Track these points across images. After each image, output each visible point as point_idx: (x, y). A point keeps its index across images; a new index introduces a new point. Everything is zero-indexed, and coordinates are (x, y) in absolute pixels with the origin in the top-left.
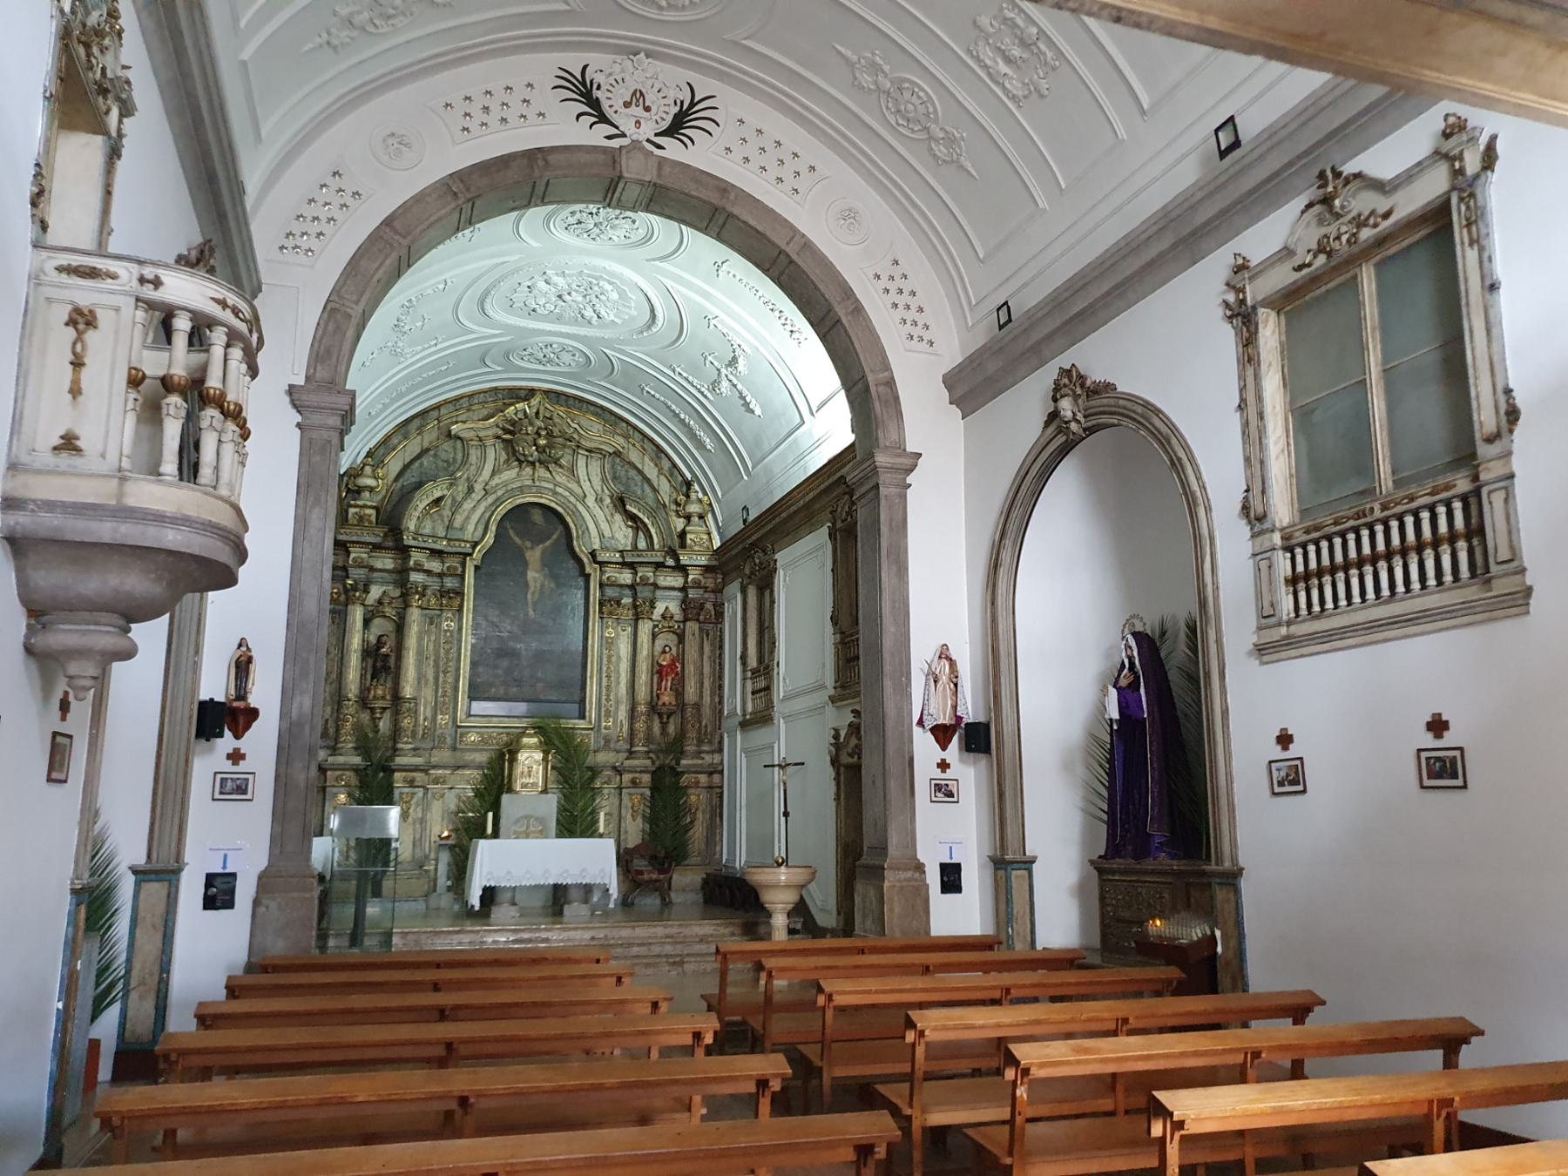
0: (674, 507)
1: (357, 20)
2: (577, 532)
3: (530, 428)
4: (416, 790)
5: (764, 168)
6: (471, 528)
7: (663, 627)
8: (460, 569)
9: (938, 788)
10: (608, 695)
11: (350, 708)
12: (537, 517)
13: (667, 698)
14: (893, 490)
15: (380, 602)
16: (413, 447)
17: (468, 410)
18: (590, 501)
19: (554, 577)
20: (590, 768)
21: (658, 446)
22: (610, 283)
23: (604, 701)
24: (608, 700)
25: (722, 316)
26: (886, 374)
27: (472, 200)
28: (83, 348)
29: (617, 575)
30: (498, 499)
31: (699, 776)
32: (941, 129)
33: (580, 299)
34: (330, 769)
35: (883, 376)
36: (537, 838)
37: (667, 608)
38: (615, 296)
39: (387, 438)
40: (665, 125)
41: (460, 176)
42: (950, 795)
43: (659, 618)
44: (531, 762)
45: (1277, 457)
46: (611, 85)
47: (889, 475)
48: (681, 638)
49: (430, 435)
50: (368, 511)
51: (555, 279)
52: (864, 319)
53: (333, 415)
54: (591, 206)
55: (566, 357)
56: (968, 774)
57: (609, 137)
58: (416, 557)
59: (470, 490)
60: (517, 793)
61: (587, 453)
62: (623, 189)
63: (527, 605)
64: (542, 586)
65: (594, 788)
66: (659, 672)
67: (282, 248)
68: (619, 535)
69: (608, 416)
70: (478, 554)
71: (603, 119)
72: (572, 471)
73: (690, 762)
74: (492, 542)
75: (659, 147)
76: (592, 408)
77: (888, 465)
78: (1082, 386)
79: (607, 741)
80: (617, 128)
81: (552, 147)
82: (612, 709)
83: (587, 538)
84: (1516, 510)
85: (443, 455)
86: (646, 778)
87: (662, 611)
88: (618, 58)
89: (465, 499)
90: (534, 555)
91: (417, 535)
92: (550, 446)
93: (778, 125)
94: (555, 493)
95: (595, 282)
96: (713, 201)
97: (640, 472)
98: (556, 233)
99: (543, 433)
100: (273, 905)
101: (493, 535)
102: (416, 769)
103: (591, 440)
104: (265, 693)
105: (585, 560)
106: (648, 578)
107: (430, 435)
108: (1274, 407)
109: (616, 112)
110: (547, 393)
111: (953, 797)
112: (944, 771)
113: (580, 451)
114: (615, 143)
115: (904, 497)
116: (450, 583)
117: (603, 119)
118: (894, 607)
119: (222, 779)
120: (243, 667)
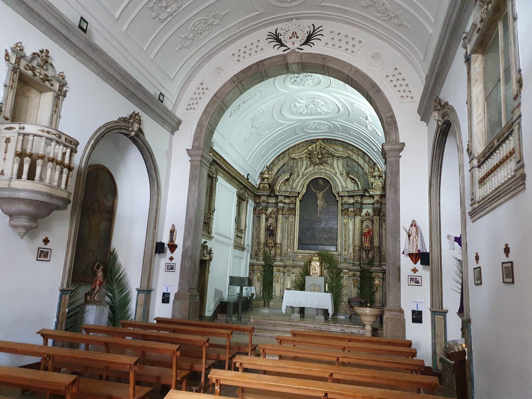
0: (370, 174)
1: (189, 37)
2: (333, 186)
3: (315, 153)
4: (281, 273)
5: (256, 51)
6: (298, 188)
7: (365, 218)
8: (295, 201)
9: (412, 279)
10: (345, 243)
11: (262, 246)
12: (321, 182)
13: (367, 244)
14: (393, 159)
15: (271, 213)
16: (281, 164)
17: (298, 149)
18: (338, 175)
19: (326, 202)
20: (339, 269)
21: (364, 152)
22: (319, 99)
23: (344, 245)
24: (345, 245)
25: (356, 102)
26: (391, 113)
27: (241, 82)
28: (7, 148)
29: (348, 200)
30: (307, 177)
31: (379, 274)
32: (393, 13)
33: (313, 106)
34: (256, 265)
35: (389, 114)
36: (318, 292)
37: (367, 211)
38: (323, 103)
39: (273, 161)
40: (303, 41)
41: (236, 76)
42: (418, 282)
43: (364, 215)
44: (316, 265)
45: (478, 124)
46: (285, 33)
47: (391, 153)
48: (373, 222)
49: (286, 159)
50: (266, 185)
51: (301, 101)
52: (381, 94)
53: (199, 157)
54: (295, 75)
55: (322, 127)
56: (424, 273)
57: (284, 51)
58: (280, 198)
59: (298, 175)
60: (311, 276)
61: (337, 158)
62: (291, 68)
63: (317, 212)
64: (323, 205)
65: (340, 276)
66: (362, 234)
67: (187, 109)
68: (349, 186)
69: (345, 144)
70: (300, 196)
71: (282, 45)
72: (332, 166)
73: (376, 268)
74: (305, 191)
75: (301, 49)
76: (339, 142)
77: (390, 149)
78: (440, 104)
79: (345, 259)
80: (287, 47)
81: (265, 59)
82: (347, 248)
83: (337, 188)
84: (522, 133)
85: (290, 165)
86: (358, 273)
87: (365, 213)
88: (287, 23)
89: (296, 178)
90: (320, 195)
91: (279, 191)
92: (323, 157)
93: (346, 29)
94: (326, 173)
95: (314, 99)
96: (320, 63)
97: (357, 162)
98: (288, 85)
99: (320, 153)
100: (177, 303)
101: (305, 189)
102: (280, 266)
103: (338, 154)
104: (179, 241)
105: (336, 196)
106: (358, 201)
107: (286, 159)
108: (478, 100)
109: (286, 42)
110: (323, 140)
111: (419, 283)
112: (171, 261)
113: (335, 158)
114: (286, 52)
115: (398, 162)
116: (292, 206)
117: (282, 45)
118: (392, 206)
119: (168, 265)
120: (172, 232)
